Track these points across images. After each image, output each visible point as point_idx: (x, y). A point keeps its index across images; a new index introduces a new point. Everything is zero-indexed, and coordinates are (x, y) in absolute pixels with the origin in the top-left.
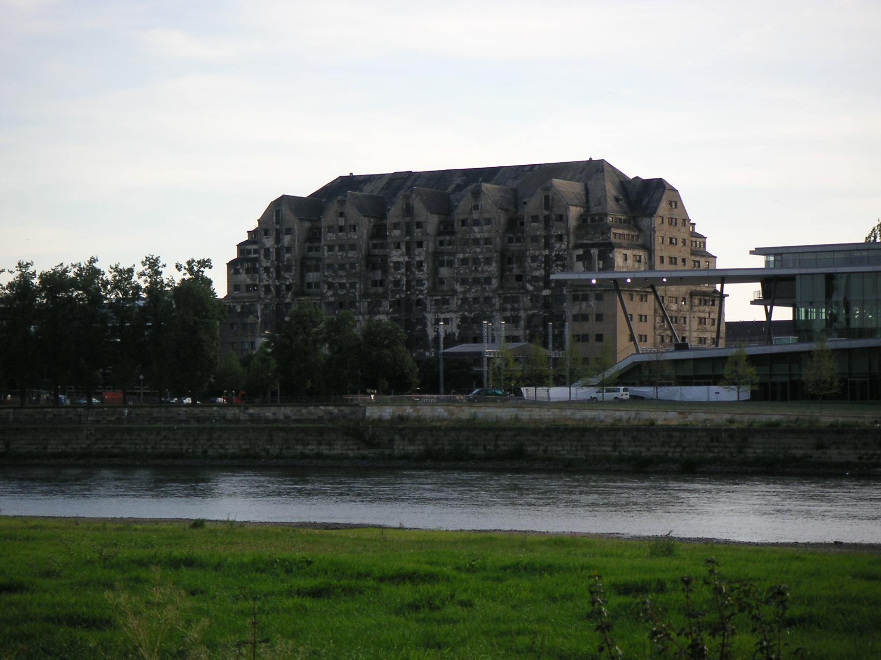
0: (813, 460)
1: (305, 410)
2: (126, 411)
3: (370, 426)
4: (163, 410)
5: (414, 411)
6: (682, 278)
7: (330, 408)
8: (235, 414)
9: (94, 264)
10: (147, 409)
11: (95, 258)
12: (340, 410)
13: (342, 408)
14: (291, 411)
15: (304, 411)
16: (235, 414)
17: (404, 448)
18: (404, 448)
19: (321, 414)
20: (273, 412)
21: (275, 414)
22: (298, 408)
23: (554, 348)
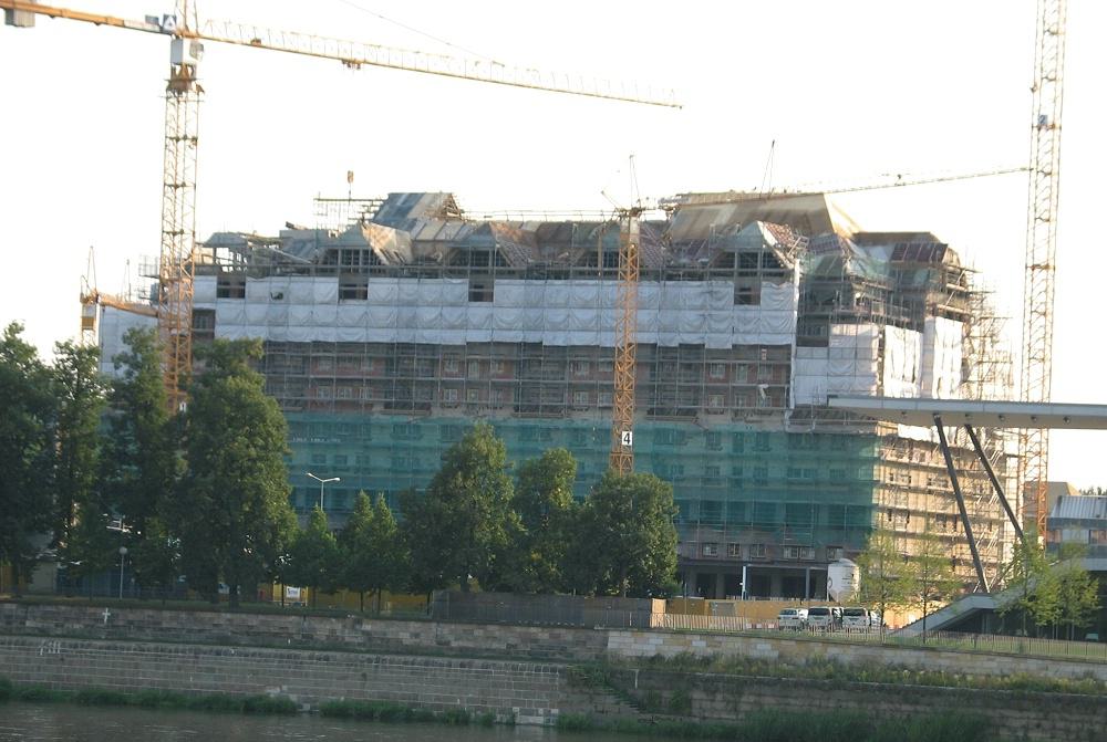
0: (722, 451)
1: (481, 631)
2: (106, 614)
3: (637, 671)
4: (183, 615)
5: (708, 646)
6: (1092, 417)
7: (533, 630)
8: (333, 631)
9: (16, 335)
10: (151, 613)
11: (20, 325)
12: (552, 636)
13: (557, 631)
14: (452, 632)
15: (478, 632)
16: (333, 631)
17: (281, 687)
18: (281, 687)
19: (512, 641)
20: (412, 630)
21: (417, 635)
22: (467, 627)
23: (342, 269)
